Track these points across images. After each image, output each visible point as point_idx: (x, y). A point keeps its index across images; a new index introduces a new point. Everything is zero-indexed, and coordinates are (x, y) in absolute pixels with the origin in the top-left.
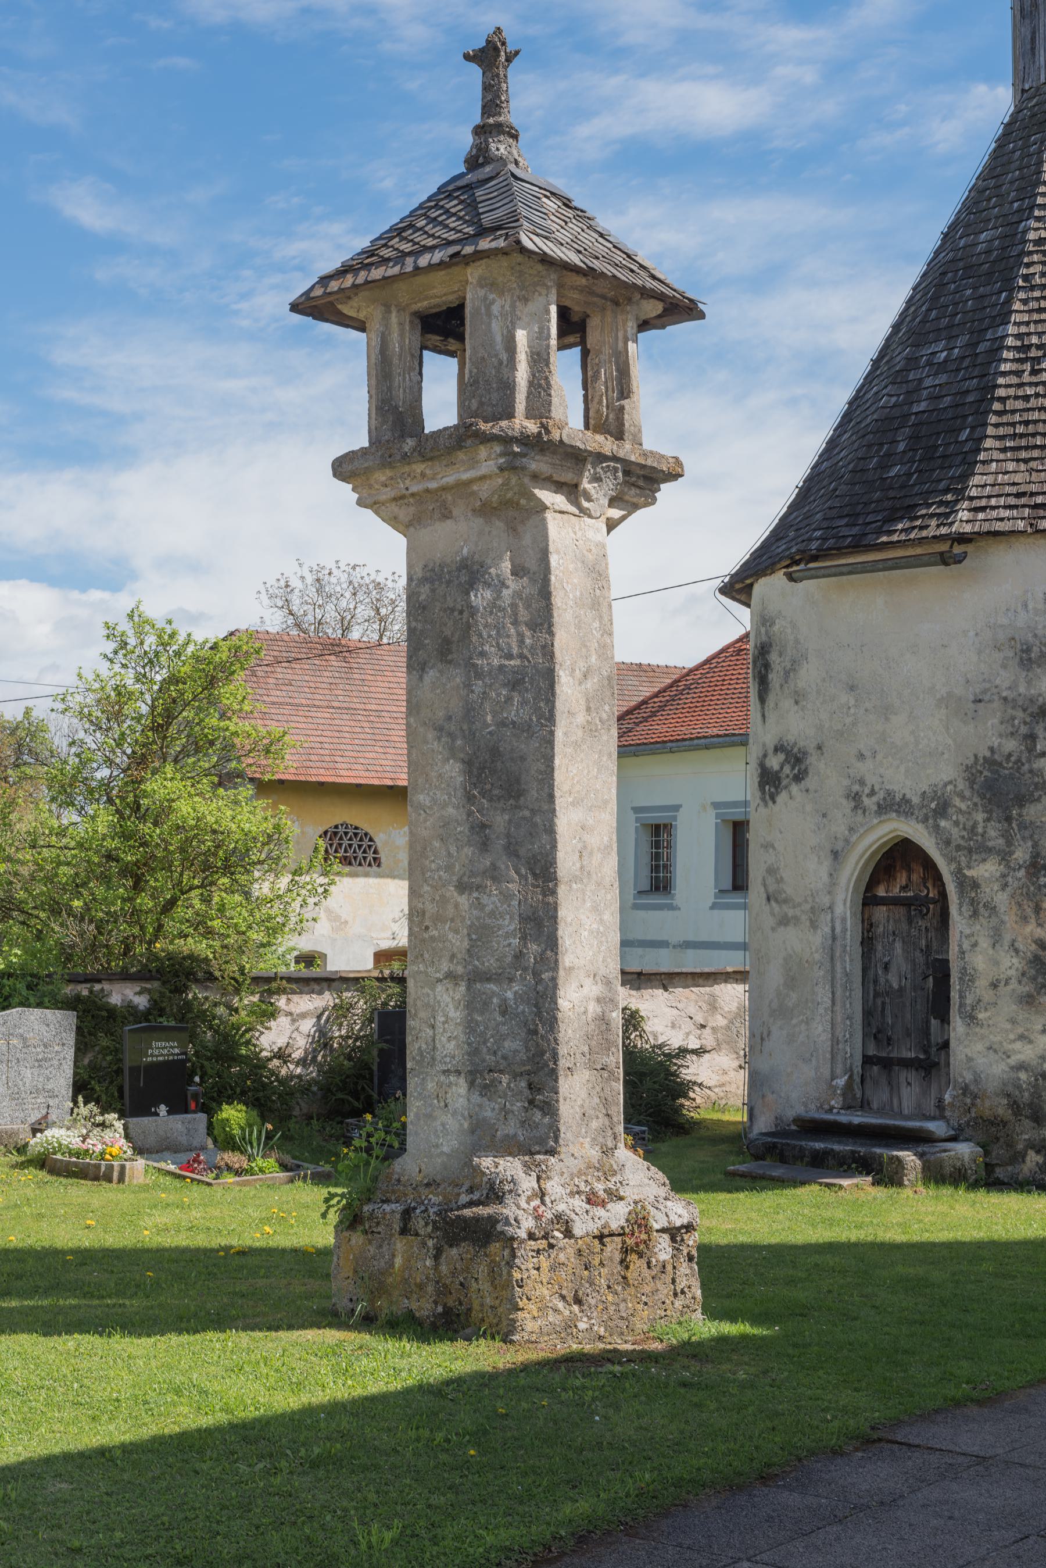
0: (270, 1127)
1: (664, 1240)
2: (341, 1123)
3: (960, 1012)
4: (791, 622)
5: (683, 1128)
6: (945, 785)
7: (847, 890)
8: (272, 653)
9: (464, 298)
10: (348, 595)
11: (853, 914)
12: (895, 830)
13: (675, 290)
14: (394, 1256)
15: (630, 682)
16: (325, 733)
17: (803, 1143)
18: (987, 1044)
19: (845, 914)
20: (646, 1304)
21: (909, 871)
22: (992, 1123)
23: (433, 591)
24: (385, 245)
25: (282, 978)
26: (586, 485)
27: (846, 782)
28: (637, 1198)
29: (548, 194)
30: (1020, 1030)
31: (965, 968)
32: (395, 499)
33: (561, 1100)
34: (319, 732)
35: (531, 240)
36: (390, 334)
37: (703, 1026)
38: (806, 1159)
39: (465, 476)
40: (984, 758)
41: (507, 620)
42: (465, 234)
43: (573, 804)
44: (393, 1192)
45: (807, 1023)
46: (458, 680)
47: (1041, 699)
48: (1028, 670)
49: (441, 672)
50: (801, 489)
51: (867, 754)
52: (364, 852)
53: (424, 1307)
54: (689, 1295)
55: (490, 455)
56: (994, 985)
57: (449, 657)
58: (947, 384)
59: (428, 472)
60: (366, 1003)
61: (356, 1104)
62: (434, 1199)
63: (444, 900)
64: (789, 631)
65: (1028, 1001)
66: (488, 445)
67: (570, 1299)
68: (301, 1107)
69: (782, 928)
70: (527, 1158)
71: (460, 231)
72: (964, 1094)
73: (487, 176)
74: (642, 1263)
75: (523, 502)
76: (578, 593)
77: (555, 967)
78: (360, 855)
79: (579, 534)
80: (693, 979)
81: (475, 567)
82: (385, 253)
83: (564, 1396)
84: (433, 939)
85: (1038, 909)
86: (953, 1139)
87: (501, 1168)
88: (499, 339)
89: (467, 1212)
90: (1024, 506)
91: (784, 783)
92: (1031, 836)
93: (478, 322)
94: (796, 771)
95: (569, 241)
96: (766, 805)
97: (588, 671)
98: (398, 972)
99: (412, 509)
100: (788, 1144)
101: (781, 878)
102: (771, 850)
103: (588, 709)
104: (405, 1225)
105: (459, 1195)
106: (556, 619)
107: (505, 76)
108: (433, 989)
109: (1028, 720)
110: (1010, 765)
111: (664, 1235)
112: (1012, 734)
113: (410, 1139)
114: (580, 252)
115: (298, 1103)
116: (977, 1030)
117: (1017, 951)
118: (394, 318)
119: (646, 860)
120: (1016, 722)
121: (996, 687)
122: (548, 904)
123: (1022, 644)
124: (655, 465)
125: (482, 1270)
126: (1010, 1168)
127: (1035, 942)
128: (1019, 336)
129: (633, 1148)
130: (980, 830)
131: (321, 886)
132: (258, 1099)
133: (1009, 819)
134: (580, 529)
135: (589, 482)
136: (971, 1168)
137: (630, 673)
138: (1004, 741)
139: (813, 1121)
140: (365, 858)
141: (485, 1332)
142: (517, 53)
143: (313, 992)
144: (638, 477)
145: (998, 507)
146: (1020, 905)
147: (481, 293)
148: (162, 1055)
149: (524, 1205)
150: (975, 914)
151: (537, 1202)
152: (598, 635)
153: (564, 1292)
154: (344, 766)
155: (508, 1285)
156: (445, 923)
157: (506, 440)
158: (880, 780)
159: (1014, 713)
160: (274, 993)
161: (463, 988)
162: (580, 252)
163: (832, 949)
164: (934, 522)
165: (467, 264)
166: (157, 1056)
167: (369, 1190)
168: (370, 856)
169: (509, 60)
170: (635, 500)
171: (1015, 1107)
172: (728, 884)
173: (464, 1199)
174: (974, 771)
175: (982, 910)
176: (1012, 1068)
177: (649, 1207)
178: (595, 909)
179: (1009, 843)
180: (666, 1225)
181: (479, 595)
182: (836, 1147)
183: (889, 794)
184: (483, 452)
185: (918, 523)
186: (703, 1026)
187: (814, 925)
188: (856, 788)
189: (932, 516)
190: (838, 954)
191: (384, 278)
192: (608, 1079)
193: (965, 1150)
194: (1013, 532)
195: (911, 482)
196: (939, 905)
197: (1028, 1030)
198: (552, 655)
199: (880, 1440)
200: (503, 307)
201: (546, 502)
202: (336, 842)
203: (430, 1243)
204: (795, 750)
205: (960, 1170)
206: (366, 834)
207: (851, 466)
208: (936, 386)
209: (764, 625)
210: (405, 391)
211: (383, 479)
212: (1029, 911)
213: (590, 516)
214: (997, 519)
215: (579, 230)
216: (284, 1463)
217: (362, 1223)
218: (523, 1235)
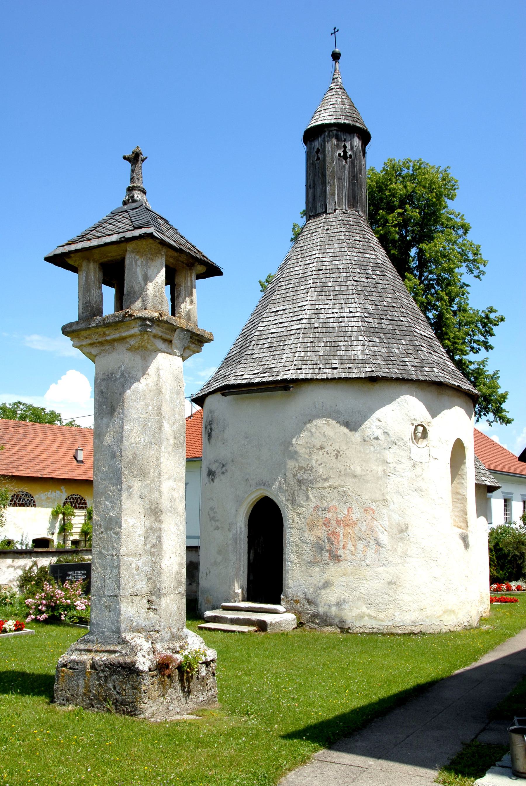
26: (176, 341)
39: (124, 334)
52: (30, 502)
59: (107, 332)
69: (216, 531)
82: (89, 236)
103: (175, 438)
111: (203, 665)
142: (146, 158)
168: (32, 503)
169: (143, 160)
178: (176, 524)
180: (204, 661)
184: (133, 324)
187: (229, 530)
202: (19, 498)
206: (30, 495)
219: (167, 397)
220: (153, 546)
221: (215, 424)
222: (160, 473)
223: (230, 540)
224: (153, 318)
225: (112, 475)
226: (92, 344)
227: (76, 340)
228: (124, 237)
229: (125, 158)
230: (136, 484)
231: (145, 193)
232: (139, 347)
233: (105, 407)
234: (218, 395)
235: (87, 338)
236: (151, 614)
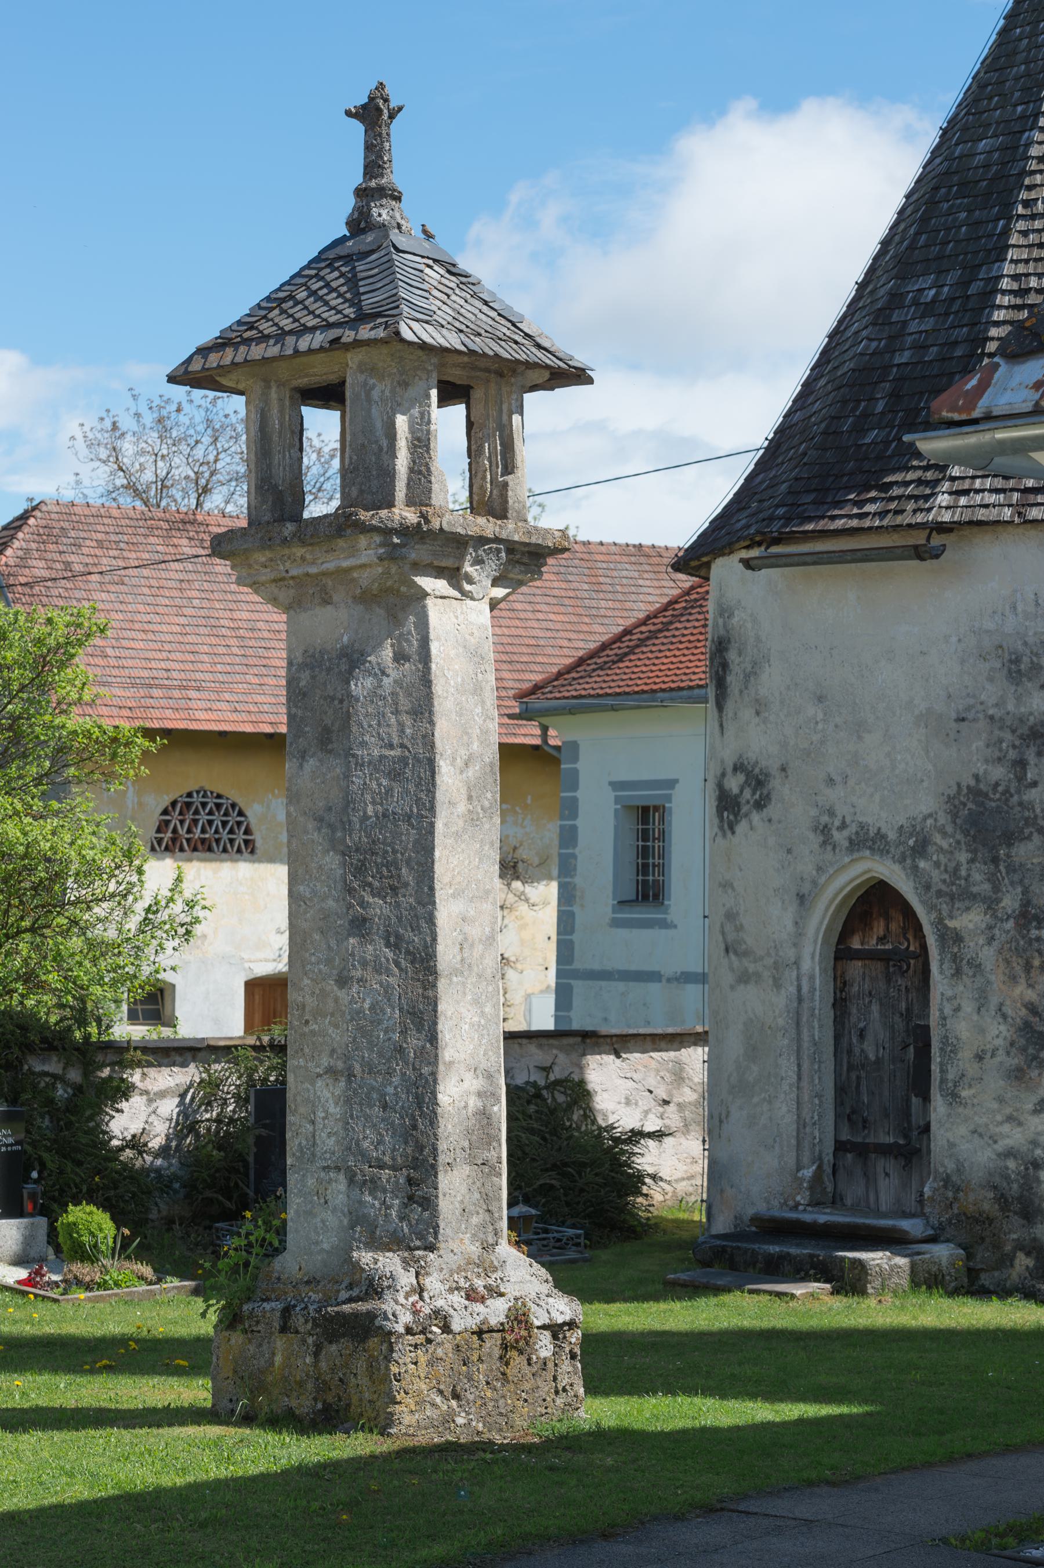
0: (127, 1232)
1: (546, 1337)
2: (210, 1228)
3: (941, 1089)
4: (752, 615)
5: (634, 1232)
6: (925, 819)
7: (815, 942)
8: (94, 536)
10: (206, 440)
11: (823, 971)
12: (869, 871)
14: (274, 1354)
15: (625, 573)
16: (172, 656)
17: (756, 1246)
18: (972, 1127)
19: (814, 970)
20: (526, 1401)
21: (888, 919)
22: (977, 1221)
23: (313, 677)
24: (265, 317)
25: (135, 1048)
27: (814, 812)
28: (518, 1294)
29: (430, 262)
30: (1008, 1111)
31: (946, 1037)
32: (275, 581)
33: (440, 1195)
34: (165, 655)
37: (666, 1102)
38: (759, 1265)
39: (345, 564)
40: (968, 787)
41: (388, 710)
42: (345, 316)
43: (453, 896)
44: (273, 1290)
45: (770, 1102)
46: (338, 770)
47: (1032, 718)
48: (1017, 685)
50: (771, 441)
51: (838, 779)
52: (231, 832)
53: (304, 1404)
54: (571, 1393)
55: (369, 544)
56: (979, 1057)
58: (934, 330)
59: (308, 556)
60: (239, 1078)
61: (228, 1204)
62: (314, 1297)
63: (324, 994)
64: (749, 625)
65: (1018, 1075)
67: (448, 1393)
68: (160, 1208)
69: (742, 986)
70: (406, 1254)
71: (339, 312)
72: (945, 1187)
73: (369, 248)
74: (523, 1359)
75: (403, 589)
77: (434, 1060)
78: (225, 835)
79: (461, 618)
80: (654, 1042)
81: (355, 656)
82: (266, 327)
83: (434, 1476)
84: (313, 1033)
85: (1028, 967)
86: (933, 1240)
87: (380, 1264)
88: (379, 425)
89: (346, 1308)
90: (1012, 490)
91: (745, 809)
92: (1021, 881)
94: (757, 796)
95: (450, 319)
97: (469, 759)
98: (279, 1039)
99: (292, 592)
100: (739, 1248)
101: (742, 925)
103: (470, 798)
104: (285, 1323)
105: (338, 1291)
106: (437, 708)
107: (388, 134)
108: (313, 1084)
109: (1017, 743)
110: (998, 796)
112: (999, 759)
113: (290, 1237)
114: (461, 331)
115: (156, 1204)
116: (960, 1110)
117: (1004, 1016)
118: (274, 395)
119: (630, 857)
120: (1004, 745)
121: (982, 703)
122: (428, 998)
123: (1010, 654)
124: (540, 542)
125: (361, 1365)
126: (996, 1274)
127: (1026, 1006)
128: (1016, 277)
129: (518, 1244)
130: (963, 873)
131: (182, 925)
132: (107, 1199)
133: (995, 860)
135: (472, 565)
136: (949, 1274)
137: (625, 559)
138: (990, 768)
139: (773, 1220)
140: (232, 841)
141: (363, 1426)
143: (174, 1065)
144: (523, 553)
145: (983, 491)
146: (1008, 962)
147: (361, 378)
149: (402, 1300)
150: (958, 973)
151: (415, 1298)
152: (479, 721)
153: (442, 1387)
154: (201, 704)
155: (386, 1379)
156: (325, 1017)
157: (387, 532)
158: (852, 810)
159: (1002, 734)
160: (126, 1067)
161: (342, 1084)
164: (910, 506)
165: (347, 350)
167: (248, 1289)
168: (240, 838)
169: (392, 117)
170: (520, 577)
171: (1003, 1200)
173: (344, 1295)
174: (957, 802)
175: (965, 968)
176: (999, 1155)
177: (530, 1304)
178: (476, 1002)
179: (996, 889)
180: (547, 1321)
182: (794, 1251)
183: (862, 828)
184: (363, 541)
185: (893, 506)
186: (666, 1102)
187: (777, 984)
188: (825, 819)
189: (910, 497)
190: (804, 1019)
192: (489, 1175)
193: (943, 1253)
194: (998, 522)
195: (889, 453)
196: (921, 960)
197: (1017, 1110)
198: (433, 746)
199: (722, 1509)
200: (383, 392)
202: (189, 817)
203: (310, 1340)
204: (757, 771)
205: (936, 1276)
206: (233, 805)
207: (823, 425)
208: (921, 332)
209: (721, 615)
212: (1019, 970)
213: (473, 599)
214: (981, 506)
215: (462, 302)
216: (176, 1524)
217: (241, 1321)
218: (401, 1329)
227: (244, 572)
229: (348, 113)
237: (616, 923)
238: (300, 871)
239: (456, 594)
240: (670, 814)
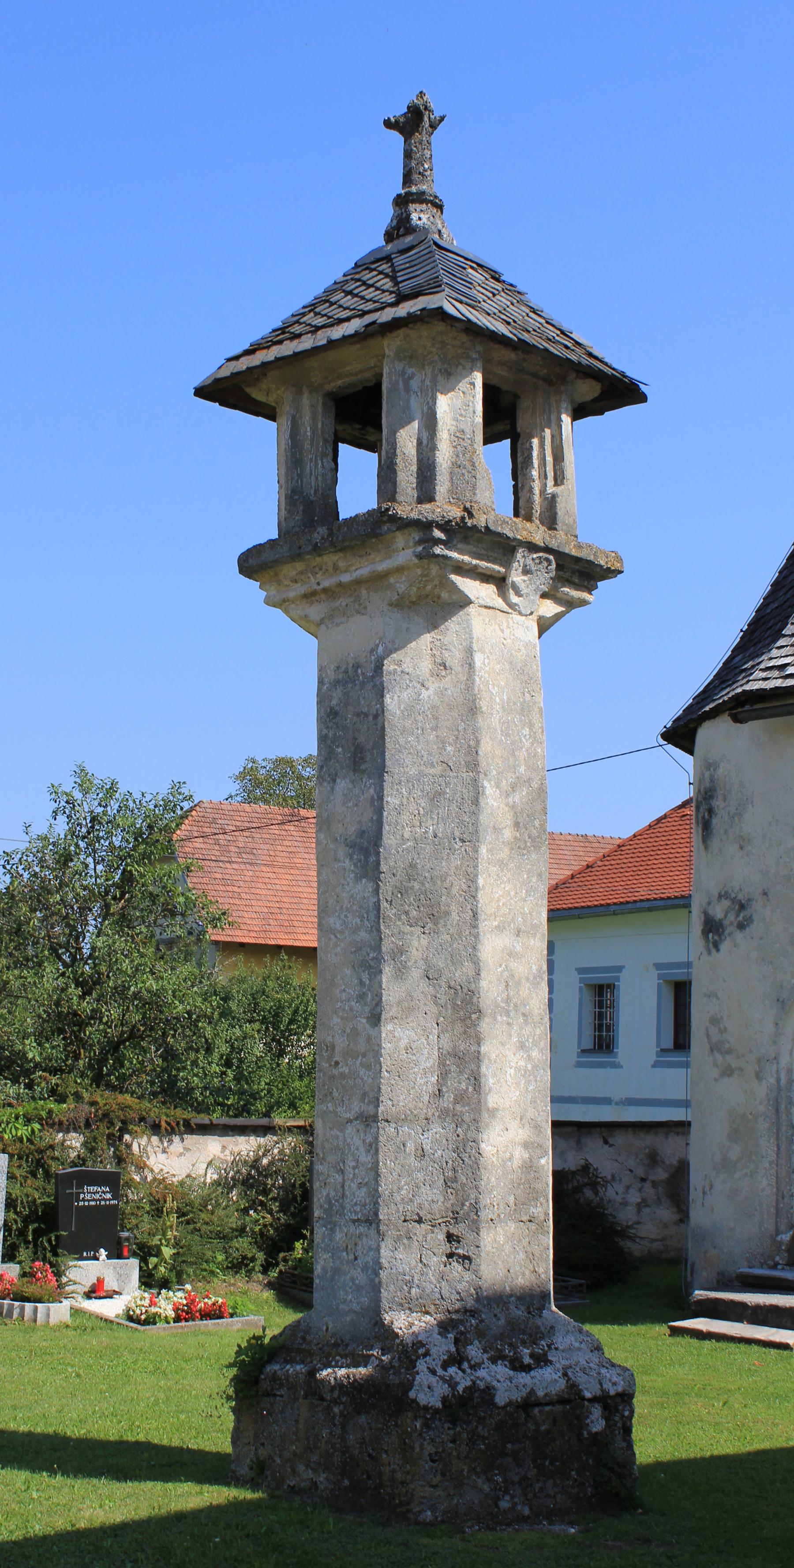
1: (596, 1412)
9: (381, 375)
13: (614, 369)
24: (297, 322)
26: (516, 577)
35: (454, 306)
36: (301, 417)
39: (382, 567)
45: (751, 1176)
49: (352, 782)
57: (363, 767)
59: (341, 564)
63: (355, 1033)
66: (406, 531)
69: (726, 1079)
76: (505, 697)
79: (507, 632)
82: (297, 329)
84: (342, 1075)
93: (400, 418)
95: (496, 311)
96: (709, 953)
101: (725, 1028)
102: (714, 999)
103: (517, 825)
108: (342, 1131)
114: (508, 323)
118: (306, 400)
119: (589, 1020)
134: (508, 627)
147: (399, 366)
148: (94, 1200)
156: (357, 1058)
162: (508, 323)
163: (777, 1100)
166: (89, 1201)
169: (433, 126)
172: (669, 1043)
178: (522, 1046)
180: (599, 1393)
181: (396, 698)
184: (400, 539)
186: (643, 1180)
187: (759, 1076)
190: (783, 1106)
191: (296, 354)
200: (423, 382)
201: (470, 596)
210: (317, 478)
211: (293, 573)
215: (509, 303)
219: (495, 721)
220: (460, 1098)
221: (720, 798)
222: (475, 915)
223: (761, 1103)
224: (450, 521)
225: (358, 920)
226: (309, 596)
228: (374, 323)
229: (388, 124)
230: (415, 943)
231: (440, 207)
232: (420, 598)
233: (340, 750)
234: (724, 723)
235: (296, 581)
236: (457, 1267)
237: (579, 1065)
238: (331, 902)
239: (499, 603)
240: (619, 990)
